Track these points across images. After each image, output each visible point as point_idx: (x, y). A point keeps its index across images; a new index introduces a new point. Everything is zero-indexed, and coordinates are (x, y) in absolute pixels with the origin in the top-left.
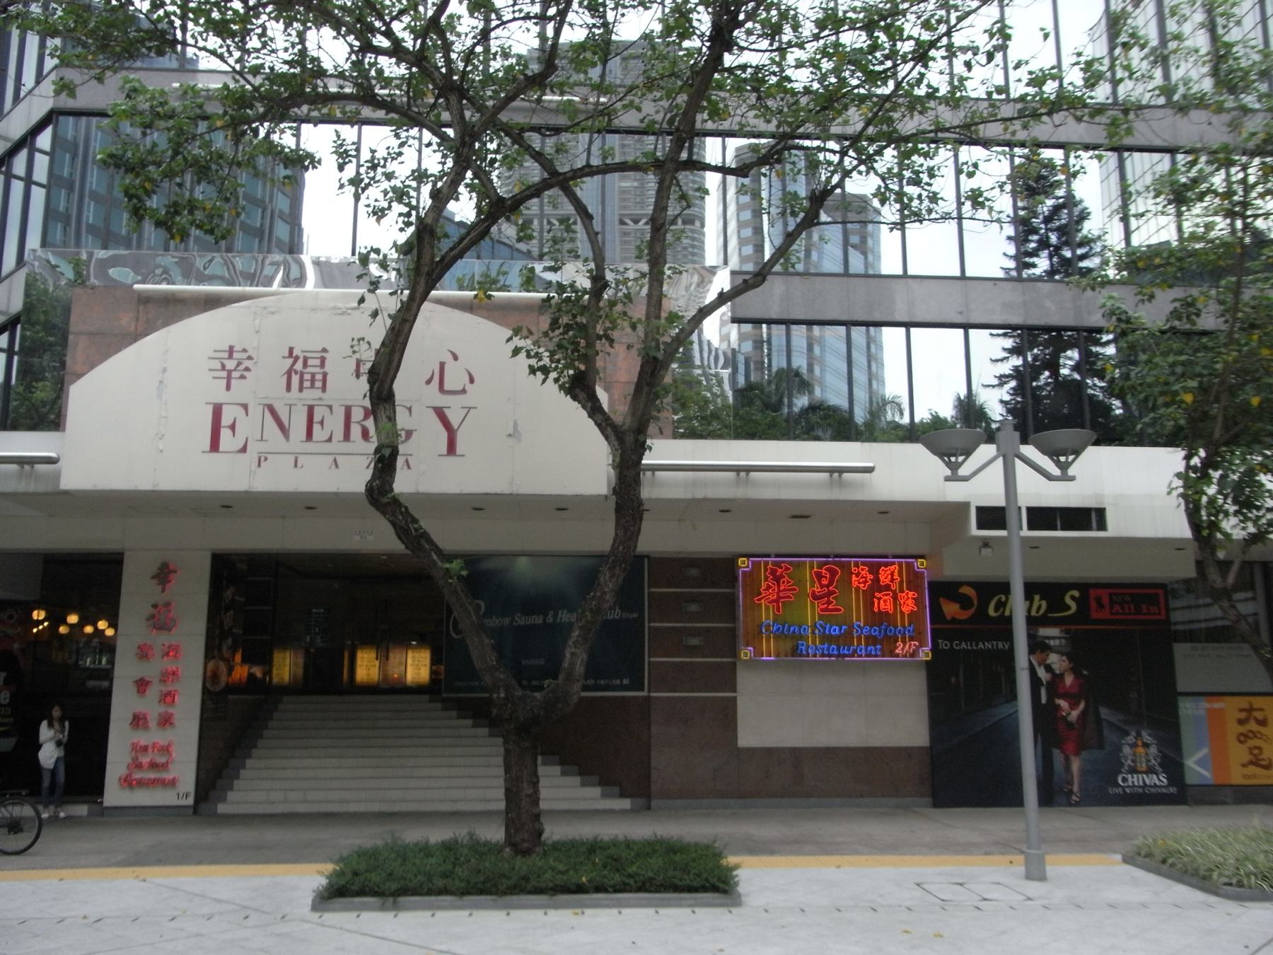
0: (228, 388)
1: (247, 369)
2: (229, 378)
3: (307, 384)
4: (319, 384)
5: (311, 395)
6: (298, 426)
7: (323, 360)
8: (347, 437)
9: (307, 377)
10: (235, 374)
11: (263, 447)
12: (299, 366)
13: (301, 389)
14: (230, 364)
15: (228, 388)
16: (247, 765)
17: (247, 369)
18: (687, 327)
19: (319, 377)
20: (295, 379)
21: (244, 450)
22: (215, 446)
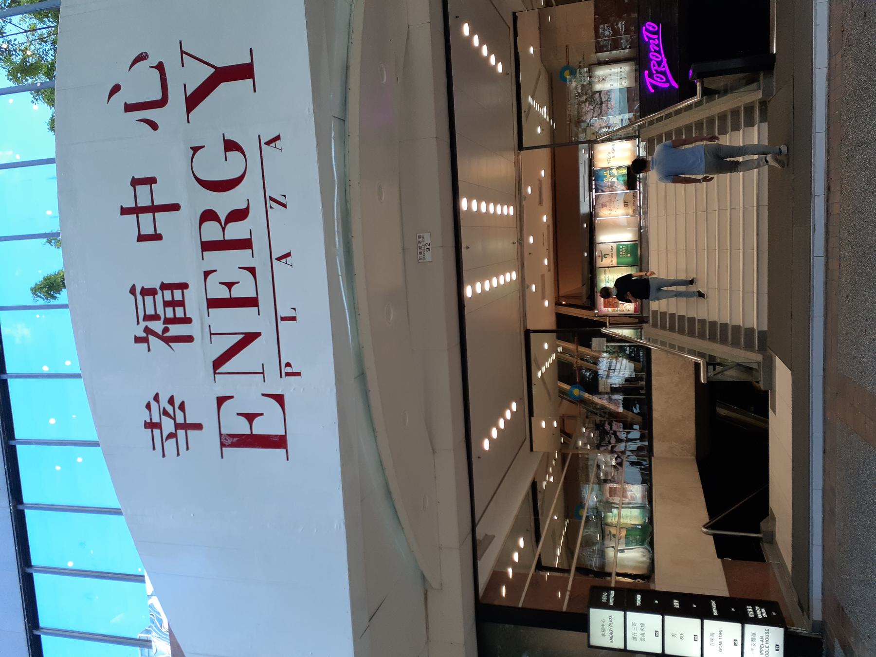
8: (245, 244)
10: (180, 419)
11: (272, 371)
13: (187, 320)
17: (171, 401)
20: (176, 330)
21: (279, 399)
22: (278, 442)
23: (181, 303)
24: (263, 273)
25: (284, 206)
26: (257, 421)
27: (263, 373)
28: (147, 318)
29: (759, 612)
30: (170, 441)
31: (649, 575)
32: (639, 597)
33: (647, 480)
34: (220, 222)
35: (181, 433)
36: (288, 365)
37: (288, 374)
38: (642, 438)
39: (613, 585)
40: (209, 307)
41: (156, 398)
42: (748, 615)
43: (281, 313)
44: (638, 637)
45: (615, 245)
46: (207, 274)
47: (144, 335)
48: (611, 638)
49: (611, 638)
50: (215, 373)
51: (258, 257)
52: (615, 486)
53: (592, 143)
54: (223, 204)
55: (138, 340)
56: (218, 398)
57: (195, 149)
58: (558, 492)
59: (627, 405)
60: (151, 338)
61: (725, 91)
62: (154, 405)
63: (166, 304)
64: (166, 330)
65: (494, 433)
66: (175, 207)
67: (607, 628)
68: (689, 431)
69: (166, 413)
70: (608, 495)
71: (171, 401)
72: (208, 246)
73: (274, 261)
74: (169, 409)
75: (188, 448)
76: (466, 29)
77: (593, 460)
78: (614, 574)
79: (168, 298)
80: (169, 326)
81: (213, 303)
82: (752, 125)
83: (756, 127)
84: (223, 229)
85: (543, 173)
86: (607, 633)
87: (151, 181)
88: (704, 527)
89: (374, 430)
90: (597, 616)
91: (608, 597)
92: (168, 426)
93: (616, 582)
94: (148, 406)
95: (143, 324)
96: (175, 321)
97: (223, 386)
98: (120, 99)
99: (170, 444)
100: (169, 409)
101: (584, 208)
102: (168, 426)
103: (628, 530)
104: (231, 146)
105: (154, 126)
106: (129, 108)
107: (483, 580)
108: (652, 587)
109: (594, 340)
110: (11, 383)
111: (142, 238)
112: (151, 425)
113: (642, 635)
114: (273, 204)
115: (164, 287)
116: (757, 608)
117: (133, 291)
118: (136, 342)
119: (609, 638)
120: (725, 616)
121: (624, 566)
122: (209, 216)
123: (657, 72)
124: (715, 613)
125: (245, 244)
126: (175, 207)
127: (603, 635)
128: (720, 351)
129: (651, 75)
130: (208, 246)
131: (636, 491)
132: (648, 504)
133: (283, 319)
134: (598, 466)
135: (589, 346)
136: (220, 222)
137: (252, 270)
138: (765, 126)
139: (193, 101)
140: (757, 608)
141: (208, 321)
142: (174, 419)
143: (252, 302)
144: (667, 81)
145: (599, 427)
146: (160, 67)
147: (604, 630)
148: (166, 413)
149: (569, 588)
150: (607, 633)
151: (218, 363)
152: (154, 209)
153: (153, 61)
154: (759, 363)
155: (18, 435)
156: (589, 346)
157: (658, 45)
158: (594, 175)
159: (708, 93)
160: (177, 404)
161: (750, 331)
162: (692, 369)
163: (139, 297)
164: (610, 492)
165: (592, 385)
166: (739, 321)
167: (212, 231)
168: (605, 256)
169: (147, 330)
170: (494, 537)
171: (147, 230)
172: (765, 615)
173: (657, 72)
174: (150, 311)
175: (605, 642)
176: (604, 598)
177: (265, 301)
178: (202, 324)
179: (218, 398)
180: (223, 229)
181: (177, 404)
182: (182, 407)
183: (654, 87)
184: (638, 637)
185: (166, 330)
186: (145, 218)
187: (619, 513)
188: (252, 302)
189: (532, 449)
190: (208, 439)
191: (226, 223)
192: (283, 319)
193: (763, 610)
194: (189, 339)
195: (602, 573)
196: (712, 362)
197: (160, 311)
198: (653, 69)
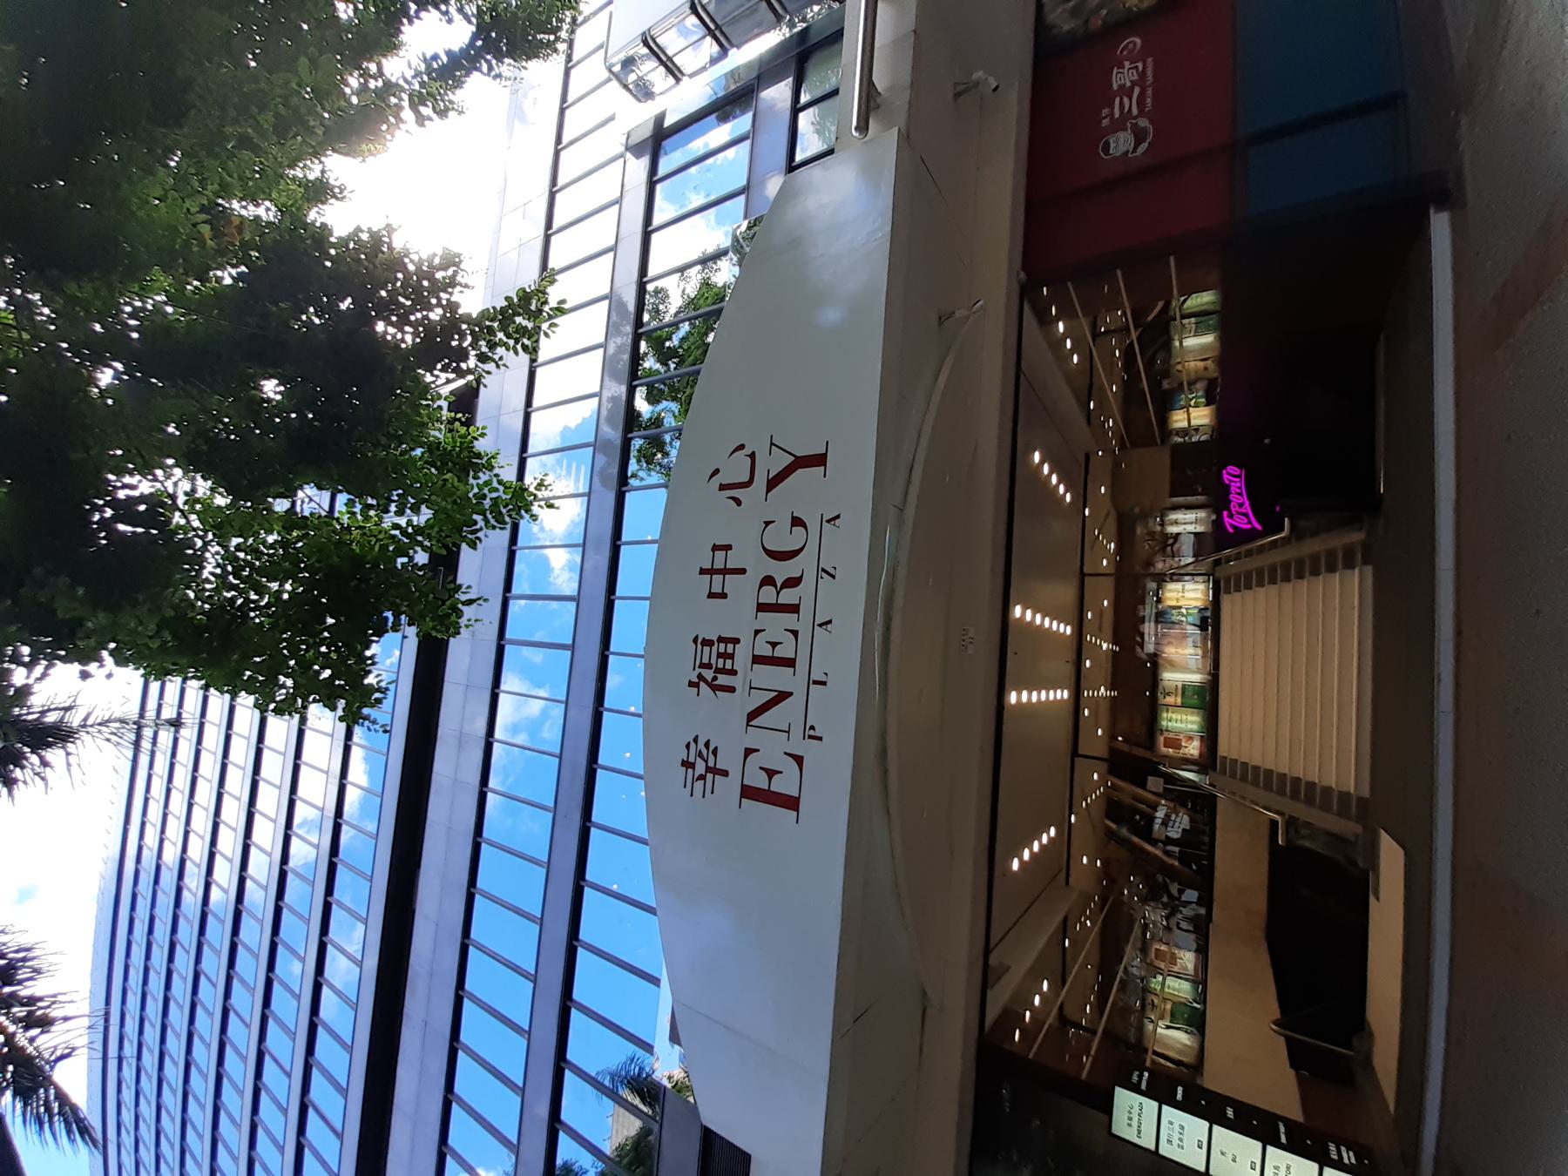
4: (730, 648)
5: (742, 654)
8: (794, 609)
10: (711, 764)
11: (797, 731)
12: (708, 674)
13: (733, 672)
17: (707, 745)
20: (723, 680)
21: (799, 760)
22: (792, 803)
23: (731, 656)
24: (804, 637)
25: (833, 577)
26: (776, 778)
27: (788, 732)
28: (702, 666)
29: (1345, 1155)
30: (699, 782)
31: (1197, 1066)
32: (1180, 1090)
33: (1202, 951)
34: (776, 587)
35: (710, 776)
36: (812, 728)
37: (811, 737)
38: (1199, 902)
39: (1148, 1064)
40: (753, 662)
41: (696, 740)
42: (1329, 1154)
43: (814, 677)
44: (1176, 1141)
45: (1180, 685)
46: (757, 632)
47: (697, 680)
48: (1139, 1132)
49: (1139, 1132)
50: (748, 725)
51: (802, 622)
52: (1163, 948)
53: (1161, 579)
54: (781, 571)
55: (691, 684)
56: (746, 749)
57: (767, 523)
58: (1092, 937)
59: (1182, 858)
60: (702, 684)
61: (1315, 534)
62: (693, 745)
63: (719, 655)
64: (715, 678)
65: (1026, 855)
66: (742, 571)
67: (1136, 1119)
68: (1260, 901)
69: (700, 755)
70: (1153, 956)
71: (707, 745)
72: (762, 608)
73: (816, 627)
74: (704, 752)
75: (712, 792)
76: (1037, 457)
77: (1138, 916)
78: (1150, 1052)
79: (722, 650)
80: (719, 676)
81: (757, 660)
82: (1353, 568)
83: (1357, 570)
84: (778, 593)
85: (1106, 603)
86: (1135, 1123)
87: (728, 548)
88: (1275, 1023)
89: (888, 814)
90: (1124, 1099)
91: (1140, 1077)
92: (700, 768)
93: (1153, 1062)
94: (688, 746)
95: (698, 670)
96: (723, 671)
97: (753, 738)
98: (717, 480)
99: (699, 784)
100: (704, 752)
101: (1150, 648)
102: (700, 768)
103: (1174, 1003)
104: (797, 522)
105: (738, 502)
106: (723, 487)
107: (991, 1017)
108: (1199, 1082)
109: (1150, 778)
110: (605, 713)
111: (711, 595)
112: (687, 764)
113: (1181, 1140)
114: (824, 575)
115: (721, 639)
116: (1343, 1149)
117: (695, 640)
118: (689, 686)
119: (1136, 1132)
120: (1294, 1147)
121: (1166, 1046)
122: (768, 581)
123: (1238, 513)
124: (1283, 1139)
125: (794, 609)
126: (742, 571)
127: (1130, 1125)
128: (1302, 812)
129: (1231, 516)
130: (762, 608)
131: (1188, 959)
132: (1200, 980)
133: (815, 682)
134: (1146, 926)
135: (1143, 786)
136: (776, 587)
137: (795, 633)
138: (1369, 570)
139: (772, 483)
140: (1343, 1149)
141: (750, 675)
142: (706, 762)
143: (790, 663)
144: (1250, 522)
145: (1148, 880)
146: (752, 456)
147: (1130, 1119)
148: (700, 755)
149: (1093, 1053)
150: (1135, 1123)
151: (752, 716)
152: (725, 572)
153: (747, 451)
154: (1356, 835)
155: (601, 761)
156: (1143, 786)
157: (1240, 488)
158: (1161, 617)
159: (1298, 534)
160: (711, 749)
161: (1345, 797)
162: (1265, 830)
163: (699, 646)
164: (1156, 955)
165: (1145, 832)
166: (1331, 781)
167: (768, 595)
168: (1168, 694)
169: (700, 676)
170: (1008, 968)
171: (717, 589)
172: (1353, 1161)
173: (1238, 513)
174: (705, 660)
175: (1129, 1134)
176: (1135, 1078)
177: (801, 664)
178: (745, 679)
179: (746, 749)
180: (778, 593)
181: (711, 749)
182: (715, 752)
183: (1233, 527)
184: (1176, 1141)
185: (715, 678)
186: (718, 578)
187: (1164, 980)
188: (790, 663)
189: (1067, 883)
190: (729, 788)
191: (781, 589)
192: (815, 682)
193: (1351, 1154)
194: (732, 689)
195: (1140, 1048)
196: (1291, 823)
197: (713, 661)
198: (1233, 510)
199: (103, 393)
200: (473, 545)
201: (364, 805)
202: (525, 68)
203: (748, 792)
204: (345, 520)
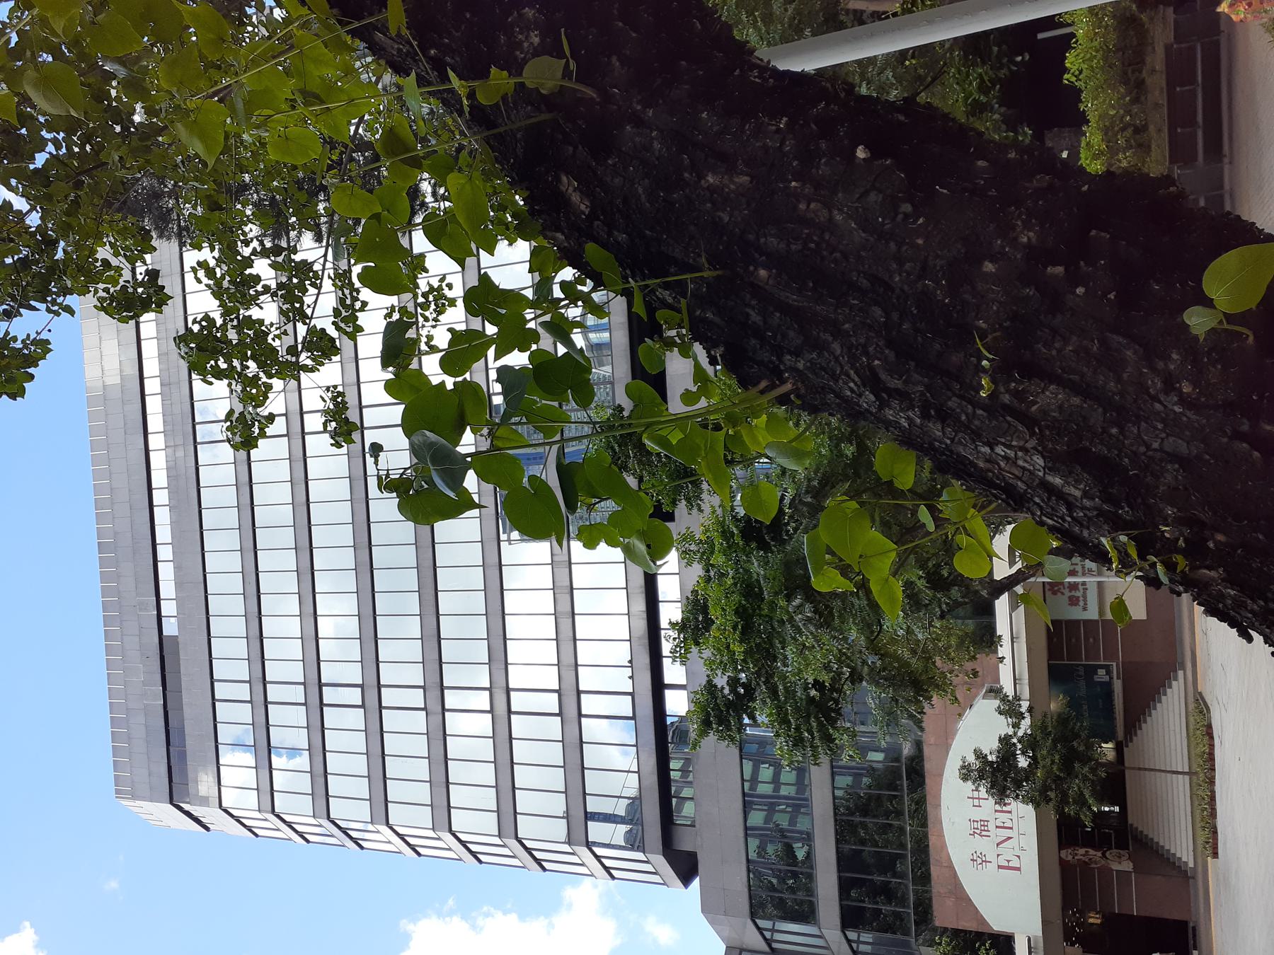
0: (990, 862)
1: (981, 854)
2: (985, 861)
3: (986, 828)
4: (986, 823)
5: (991, 826)
6: (1008, 833)
7: (974, 821)
8: (1010, 812)
9: (983, 828)
10: (984, 859)
11: (1017, 848)
12: (978, 831)
13: (988, 831)
14: (979, 861)
15: (990, 862)
16: (1186, 860)
17: (981, 854)
18: (828, 469)
19: (982, 823)
20: (984, 833)
21: (1019, 857)
22: (1018, 869)
130: (996, 811)
143: (1011, 828)
190: (992, 867)
199: (981, 378)
200: (1001, 646)
201: (181, 615)
202: (71, 311)
203: (1000, 867)
204: (309, 249)
